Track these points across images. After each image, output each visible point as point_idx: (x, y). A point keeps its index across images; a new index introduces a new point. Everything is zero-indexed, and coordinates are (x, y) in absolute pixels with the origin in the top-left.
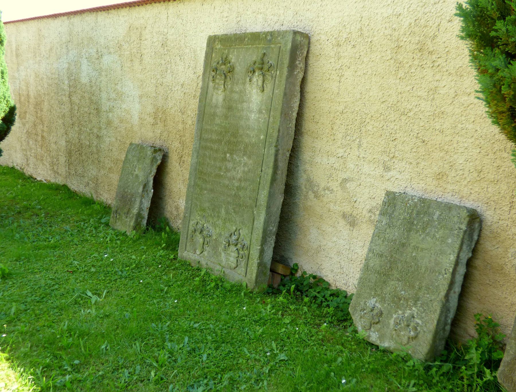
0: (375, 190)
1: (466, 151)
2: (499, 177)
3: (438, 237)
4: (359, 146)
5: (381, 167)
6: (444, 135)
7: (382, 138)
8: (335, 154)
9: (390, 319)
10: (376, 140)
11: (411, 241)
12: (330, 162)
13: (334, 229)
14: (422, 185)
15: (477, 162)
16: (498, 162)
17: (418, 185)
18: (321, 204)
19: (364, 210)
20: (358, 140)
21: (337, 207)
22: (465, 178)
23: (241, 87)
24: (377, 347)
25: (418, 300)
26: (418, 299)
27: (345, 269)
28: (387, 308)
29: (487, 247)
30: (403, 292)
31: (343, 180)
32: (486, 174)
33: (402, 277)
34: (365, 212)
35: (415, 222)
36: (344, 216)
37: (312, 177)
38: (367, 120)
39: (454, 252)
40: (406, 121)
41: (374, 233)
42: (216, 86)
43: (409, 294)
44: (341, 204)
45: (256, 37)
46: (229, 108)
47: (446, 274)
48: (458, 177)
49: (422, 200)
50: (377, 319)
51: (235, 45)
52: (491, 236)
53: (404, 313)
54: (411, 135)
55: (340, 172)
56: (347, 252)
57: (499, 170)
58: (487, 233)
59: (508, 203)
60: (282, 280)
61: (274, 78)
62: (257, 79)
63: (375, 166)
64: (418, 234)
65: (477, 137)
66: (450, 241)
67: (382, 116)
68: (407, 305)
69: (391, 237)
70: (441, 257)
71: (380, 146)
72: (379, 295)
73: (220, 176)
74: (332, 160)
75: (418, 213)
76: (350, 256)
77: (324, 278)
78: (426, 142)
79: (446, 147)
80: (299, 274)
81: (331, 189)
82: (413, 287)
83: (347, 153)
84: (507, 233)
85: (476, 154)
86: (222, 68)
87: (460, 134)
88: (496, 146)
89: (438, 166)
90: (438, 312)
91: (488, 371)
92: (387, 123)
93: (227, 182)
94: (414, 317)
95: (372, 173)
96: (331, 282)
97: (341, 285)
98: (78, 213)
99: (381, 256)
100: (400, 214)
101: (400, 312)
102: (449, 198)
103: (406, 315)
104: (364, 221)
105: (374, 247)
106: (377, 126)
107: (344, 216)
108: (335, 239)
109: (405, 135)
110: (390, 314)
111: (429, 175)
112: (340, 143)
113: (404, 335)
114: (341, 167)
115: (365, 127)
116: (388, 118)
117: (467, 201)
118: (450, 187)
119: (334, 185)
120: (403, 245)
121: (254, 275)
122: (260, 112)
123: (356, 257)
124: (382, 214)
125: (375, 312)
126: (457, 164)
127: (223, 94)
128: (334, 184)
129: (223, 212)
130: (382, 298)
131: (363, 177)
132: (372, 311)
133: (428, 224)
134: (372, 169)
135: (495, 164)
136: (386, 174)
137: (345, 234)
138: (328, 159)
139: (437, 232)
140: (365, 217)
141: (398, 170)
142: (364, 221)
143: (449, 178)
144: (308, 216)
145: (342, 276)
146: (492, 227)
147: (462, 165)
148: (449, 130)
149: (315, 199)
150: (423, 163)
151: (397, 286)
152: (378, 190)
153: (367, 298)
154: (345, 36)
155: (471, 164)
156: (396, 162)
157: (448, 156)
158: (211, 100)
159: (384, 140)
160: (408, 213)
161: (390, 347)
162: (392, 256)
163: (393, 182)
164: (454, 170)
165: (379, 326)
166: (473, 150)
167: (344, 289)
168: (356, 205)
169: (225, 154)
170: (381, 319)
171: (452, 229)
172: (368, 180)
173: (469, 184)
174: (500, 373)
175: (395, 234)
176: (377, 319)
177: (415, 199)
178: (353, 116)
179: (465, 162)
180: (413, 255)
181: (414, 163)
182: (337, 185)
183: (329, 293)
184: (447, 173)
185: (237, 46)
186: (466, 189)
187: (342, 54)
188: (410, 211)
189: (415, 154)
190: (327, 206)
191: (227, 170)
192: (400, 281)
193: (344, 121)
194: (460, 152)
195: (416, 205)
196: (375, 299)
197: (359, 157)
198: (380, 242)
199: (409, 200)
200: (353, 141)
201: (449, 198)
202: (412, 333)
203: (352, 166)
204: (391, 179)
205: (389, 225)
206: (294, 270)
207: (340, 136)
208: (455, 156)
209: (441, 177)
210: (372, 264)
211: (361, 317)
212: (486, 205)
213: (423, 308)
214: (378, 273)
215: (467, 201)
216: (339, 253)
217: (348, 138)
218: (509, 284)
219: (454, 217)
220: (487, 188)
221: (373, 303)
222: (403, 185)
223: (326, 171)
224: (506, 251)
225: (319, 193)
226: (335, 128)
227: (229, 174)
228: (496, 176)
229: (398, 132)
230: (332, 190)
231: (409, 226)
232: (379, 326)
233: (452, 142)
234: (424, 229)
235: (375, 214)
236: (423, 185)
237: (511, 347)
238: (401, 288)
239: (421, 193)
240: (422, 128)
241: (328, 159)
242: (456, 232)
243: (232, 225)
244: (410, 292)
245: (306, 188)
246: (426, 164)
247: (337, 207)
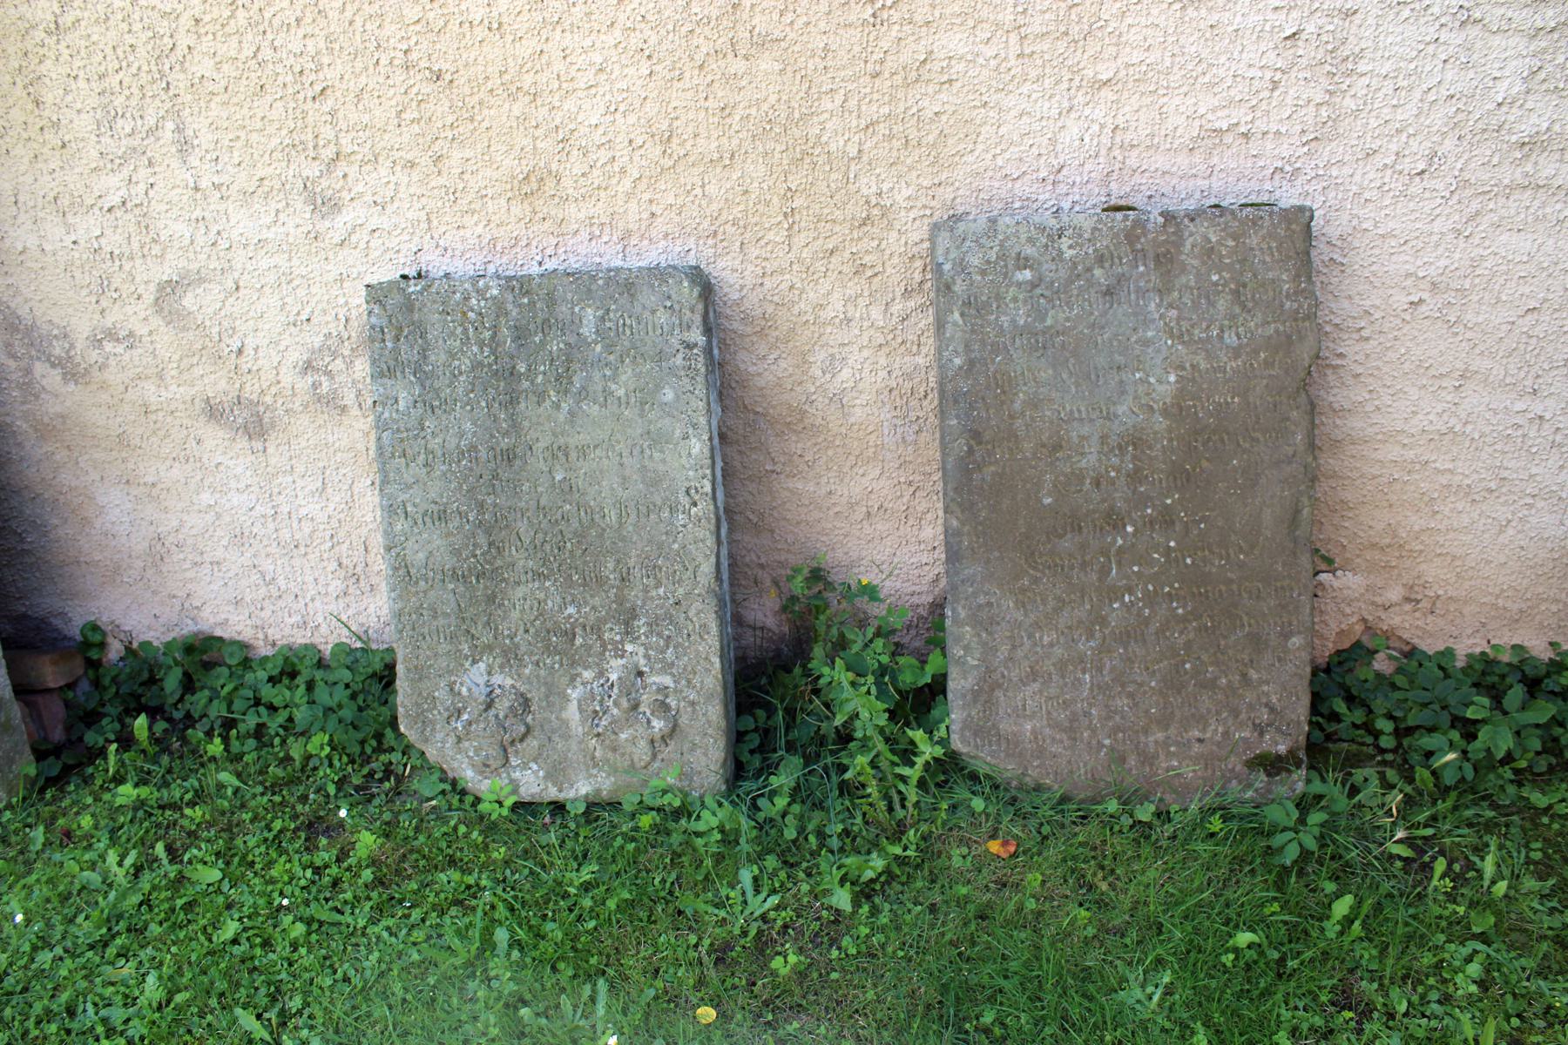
0: (301, 292)
1: (603, 77)
2: (735, 142)
3: (621, 392)
4: (184, 146)
5: (299, 205)
6: (509, 38)
7: (269, 99)
8: (89, 202)
9: (562, 709)
10: (245, 111)
11: (533, 435)
12: (80, 234)
13: (189, 467)
14: (475, 229)
15: (651, 109)
16: (720, 94)
17: (462, 232)
18: (104, 397)
19: (283, 370)
20: (170, 126)
21: (173, 388)
22: (623, 171)
24: (558, 808)
25: (635, 617)
26: (633, 614)
27: (281, 582)
28: (538, 676)
29: (742, 367)
30: (571, 610)
31: (161, 287)
32: (691, 142)
33: (545, 561)
34: (288, 377)
35: (522, 368)
36: (213, 412)
37: (23, 312)
38: (184, 41)
39: (695, 426)
40: (348, 14)
41: (380, 448)
43: (594, 608)
44: (186, 376)
47: (695, 504)
48: (596, 173)
49: (519, 285)
50: (518, 724)
52: (749, 330)
53: (601, 674)
54: (382, 62)
55: (139, 262)
56: (271, 526)
57: (728, 121)
58: (735, 325)
59: (781, 218)
60: (67, 704)
63: (274, 205)
64: (548, 403)
65: (629, 24)
66: (669, 395)
67: (241, 13)
68: (604, 645)
69: (452, 442)
70: (657, 455)
71: (271, 129)
72: (489, 648)
74: (88, 226)
75: (520, 334)
76: (285, 534)
77: (218, 633)
78: (448, 77)
79: (528, 79)
80: (115, 650)
81: (122, 334)
82: (601, 581)
83: (142, 187)
84: (796, 310)
85: (639, 82)
87: (566, 25)
88: (701, 40)
89: (516, 152)
90: (714, 628)
91: (918, 735)
92: (270, 36)
94: (640, 674)
95: (271, 236)
96: (247, 635)
97: (287, 631)
99: (442, 516)
100: (452, 355)
101: (588, 675)
102: (582, 250)
103: (614, 677)
104: (297, 406)
105: (402, 497)
106: (233, 53)
107: (213, 412)
108: (206, 498)
109: (359, 65)
110: (556, 697)
111: (490, 192)
112: (94, 154)
113: (633, 741)
114: (135, 245)
115: (184, 71)
116: (267, 15)
117: (646, 242)
118: (575, 213)
119: (134, 315)
120: (509, 456)
123: (307, 531)
124: (385, 371)
125: (502, 707)
126: (583, 130)
128: (129, 310)
130: (505, 653)
131: (239, 257)
132: (489, 706)
133: (569, 361)
134: (269, 219)
135: (711, 103)
136: (327, 224)
137: (239, 470)
138: (69, 228)
139: (614, 378)
140: (294, 395)
141: (369, 198)
142: (297, 406)
143: (567, 182)
144: (65, 452)
145: (281, 603)
146: (747, 304)
147: (601, 131)
148: (525, 16)
149: (72, 387)
150: (457, 155)
151: (542, 596)
152: (313, 290)
153: (450, 672)
155: (632, 119)
156: (353, 171)
157: (544, 111)
159: (279, 104)
160: (481, 344)
161: (598, 791)
162: (481, 506)
163: (362, 245)
164: (575, 152)
165: (535, 743)
166: (626, 71)
167: (303, 641)
168: (246, 362)
170: (529, 719)
171: (660, 357)
172: (264, 263)
173: (642, 186)
174: (962, 729)
175: (462, 426)
176: (518, 724)
177: (488, 287)
178: (112, 34)
179: (609, 118)
180: (558, 478)
181: (425, 161)
182: (142, 315)
183: (262, 675)
184: (554, 166)
186: (633, 205)
188: (487, 334)
189: (416, 128)
190: (131, 395)
192: (547, 578)
193: (77, 63)
194: (583, 86)
195: (499, 308)
196: (482, 666)
197: (197, 189)
198: (417, 470)
199: (467, 299)
200: (150, 132)
201: (582, 250)
202: (658, 724)
203: (182, 229)
204: (354, 239)
205: (430, 403)
206: (90, 644)
207: (84, 124)
208: (570, 105)
209: (535, 186)
210: (421, 555)
211: (459, 740)
212: (710, 242)
213: (659, 635)
214: (455, 576)
215: (646, 242)
216: (240, 538)
217: (124, 126)
218: (830, 453)
219: (653, 312)
220: (703, 186)
221: (481, 681)
222: (404, 247)
223: (78, 274)
224: (804, 360)
225: (78, 359)
226: (49, 98)
228: (724, 140)
229: (326, 60)
230: (131, 334)
231: (504, 382)
232: (535, 743)
233: (544, 58)
234: (562, 381)
235: (329, 373)
236: (479, 230)
237: (967, 648)
238: (559, 599)
239: (479, 259)
240: (418, 28)
241: (69, 228)
242: (679, 360)
244: (597, 601)
245: (14, 357)
246: (468, 153)
247: (173, 388)
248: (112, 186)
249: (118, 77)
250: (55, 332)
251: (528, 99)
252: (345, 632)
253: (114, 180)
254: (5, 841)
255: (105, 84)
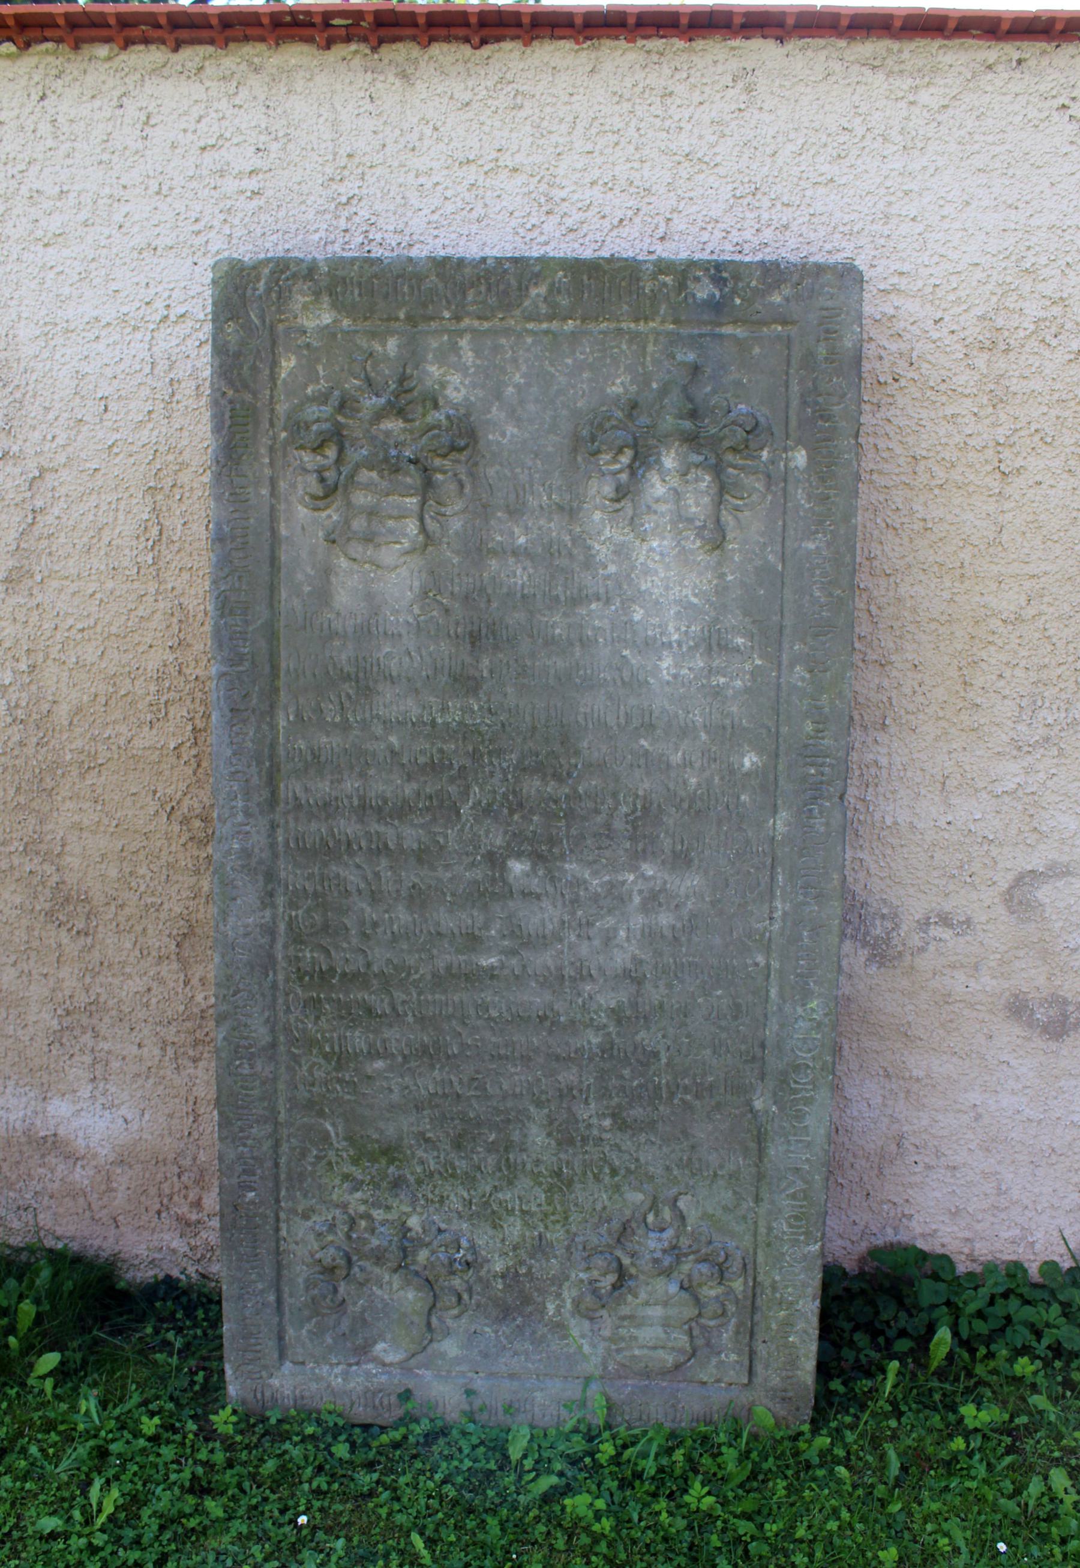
23: (554, 528)
36: (1018, 1008)
42: (359, 524)
45: (600, 287)
46: (474, 638)
51: (458, 318)
61: (778, 480)
62: (672, 483)
73: (474, 978)
86: (388, 434)
93: (535, 998)
98: (946, 1489)
108: (974, 1097)
121: (809, 1364)
122: (713, 643)
127: (416, 562)
129: (538, 1137)
149: (873, 969)
154: (1033, 309)
158: (323, 595)
169: (495, 861)
185: (466, 322)
187: (1015, 385)
191: (524, 941)
226: (979, 682)
227: (544, 960)
230: (968, 922)
243: (617, 1188)
248: (1011, 773)
249: (1059, 671)
250: (885, 911)
251: (1007, 453)
252: (1063, 1249)
253: (1013, 767)
254: (650, 1565)
255: (1044, 675)
